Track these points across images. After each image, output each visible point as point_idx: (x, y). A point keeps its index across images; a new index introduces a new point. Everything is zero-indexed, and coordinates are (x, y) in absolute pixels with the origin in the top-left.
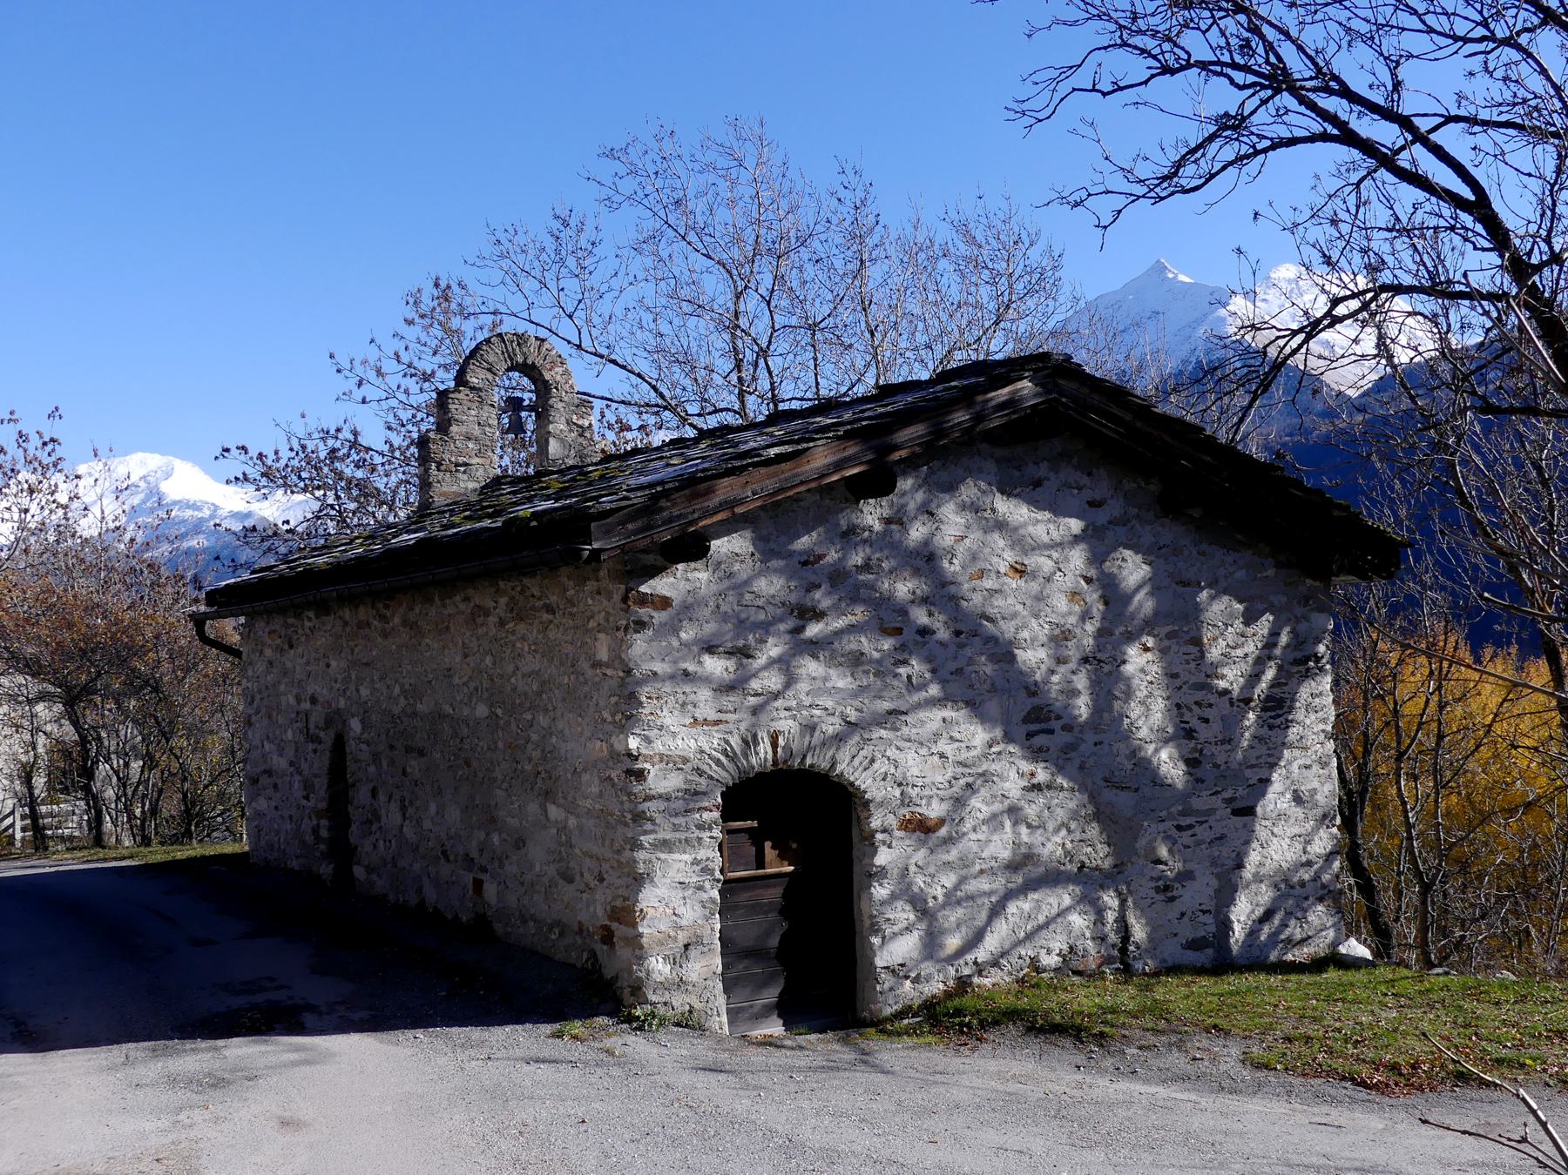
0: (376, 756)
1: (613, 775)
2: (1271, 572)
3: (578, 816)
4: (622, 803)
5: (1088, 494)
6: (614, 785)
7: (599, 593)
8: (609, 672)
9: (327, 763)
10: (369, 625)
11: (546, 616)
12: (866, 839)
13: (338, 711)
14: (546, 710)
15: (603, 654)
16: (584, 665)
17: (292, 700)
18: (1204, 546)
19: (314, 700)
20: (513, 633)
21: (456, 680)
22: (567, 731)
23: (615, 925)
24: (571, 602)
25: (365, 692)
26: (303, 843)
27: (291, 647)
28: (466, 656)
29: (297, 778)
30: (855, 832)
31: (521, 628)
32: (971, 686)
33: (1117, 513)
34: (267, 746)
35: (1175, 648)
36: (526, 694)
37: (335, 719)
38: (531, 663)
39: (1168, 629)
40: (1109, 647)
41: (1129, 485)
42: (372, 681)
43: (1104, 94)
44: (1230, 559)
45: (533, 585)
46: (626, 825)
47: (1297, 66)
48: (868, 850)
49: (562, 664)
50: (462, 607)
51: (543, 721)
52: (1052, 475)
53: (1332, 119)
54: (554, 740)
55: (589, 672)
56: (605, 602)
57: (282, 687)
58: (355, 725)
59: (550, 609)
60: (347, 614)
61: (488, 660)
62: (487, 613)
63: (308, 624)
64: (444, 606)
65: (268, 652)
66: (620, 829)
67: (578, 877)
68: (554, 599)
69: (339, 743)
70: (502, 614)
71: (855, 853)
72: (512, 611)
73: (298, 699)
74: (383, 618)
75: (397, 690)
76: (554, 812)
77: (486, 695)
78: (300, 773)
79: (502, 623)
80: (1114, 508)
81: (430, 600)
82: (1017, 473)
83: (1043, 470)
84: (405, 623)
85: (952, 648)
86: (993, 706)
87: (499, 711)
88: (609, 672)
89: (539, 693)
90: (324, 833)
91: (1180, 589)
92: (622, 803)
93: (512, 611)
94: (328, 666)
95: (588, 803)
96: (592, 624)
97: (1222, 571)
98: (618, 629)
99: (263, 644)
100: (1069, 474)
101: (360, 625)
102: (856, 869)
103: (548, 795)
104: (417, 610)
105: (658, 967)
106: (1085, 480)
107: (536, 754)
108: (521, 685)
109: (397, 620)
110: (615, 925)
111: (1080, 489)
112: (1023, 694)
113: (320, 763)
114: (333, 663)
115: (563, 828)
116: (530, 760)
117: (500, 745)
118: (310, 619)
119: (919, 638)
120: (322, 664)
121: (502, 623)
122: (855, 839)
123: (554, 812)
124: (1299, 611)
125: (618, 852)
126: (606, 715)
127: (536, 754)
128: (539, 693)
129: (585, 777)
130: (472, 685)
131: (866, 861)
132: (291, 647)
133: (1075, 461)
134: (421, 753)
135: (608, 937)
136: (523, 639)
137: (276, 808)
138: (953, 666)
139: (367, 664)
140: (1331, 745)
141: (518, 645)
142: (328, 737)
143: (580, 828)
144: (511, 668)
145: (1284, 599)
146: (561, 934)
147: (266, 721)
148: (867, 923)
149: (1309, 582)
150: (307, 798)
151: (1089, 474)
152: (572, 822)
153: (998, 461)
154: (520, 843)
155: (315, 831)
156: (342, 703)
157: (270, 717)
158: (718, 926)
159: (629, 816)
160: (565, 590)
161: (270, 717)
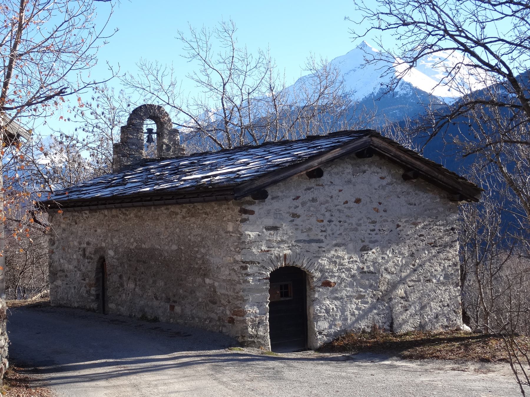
0: (122, 264)
1: (235, 268)
2: (438, 200)
3: (219, 282)
4: (239, 277)
5: (380, 175)
6: (235, 271)
7: (228, 209)
8: (233, 235)
9: (95, 266)
10: (117, 216)
11: (204, 216)
12: (311, 289)
13: (102, 248)
14: (204, 247)
15: (230, 229)
16: (222, 232)
17: (76, 243)
18: (417, 192)
19: (88, 243)
20: (189, 221)
21: (162, 237)
22: (214, 254)
23: (235, 317)
24: (216, 211)
25: (115, 241)
26: (82, 296)
27: (76, 224)
28: (166, 228)
29: (79, 272)
30: (308, 287)
31: (193, 219)
32: (344, 239)
33: (389, 181)
34: (62, 261)
35: (408, 226)
36: (195, 242)
37: (99, 250)
38: (197, 231)
39: (406, 219)
40: (387, 226)
41: (393, 172)
42: (119, 237)
43: (383, 30)
44: (425, 196)
45: (199, 206)
46: (240, 284)
47: (450, 28)
48: (312, 293)
49: (212, 232)
50: (165, 211)
51: (203, 250)
52: (369, 169)
53: (462, 44)
54: (208, 257)
55: (224, 235)
56: (231, 212)
57: (71, 239)
58: (111, 253)
59: (206, 213)
60: (106, 212)
61: (177, 230)
62: (177, 214)
63: (85, 215)
64: (156, 211)
65: (63, 226)
66: (238, 285)
67: (218, 302)
68: (208, 210)
69: (102, 261)
70: (184, 215)
71: (308, 294)
72: (188, 213)
73: (80, 243)
74: (125, 214)
75: (132, 240)
76: (207, 281)
77: (176, 242)
78: (80, 271)
79: (184, 217)
80: (389, 179)
81: (150, 210)
82: (358, 169)
83: (366, 167)
84: (136, 216)
85: (339, 226)
86: (351, 246)
87: (182, 248)
88: (233, 235)
89: (201, 242)
90: (93, 292)
91: (409, 206)
92: (239, 277)
93: (188, 213)
94: (96, 231)
95: (224, 278)
96: (225, 219)
97: (423, 200)
98: (237, 221)
99: (60, 222)
100: (374, 169)
101: (113, 216)
102: (308, 299)
103: (205, 275)
104: (142, 212)
105: (251, 331)
106: (379, 170)
107: (200, 262)
108: (193, 239)
109: (132, 215)
110: (235, 317)
111: (377, 173)
112: (360, 241)
113: (90, 267)
114: (99, 230)
115: (212, 286)
116: (197, 263)
117: (183, 259)
118: (86, 214)
119: (328, 223)
120: (92, 231)
121: (184, 217)
122: (308, 289)
123: (207, 281)
124: (447, 213)
125: (237, 293)
126: (232, 249)
127: (200, 262)
128: (201, 242)
129: (222, 269)
130: (169, 239)
131: (312, 296)
132: (76, 224)
133: (376, 164)
134: (144, 262)
135: (232, 321)
136: (194, 223)
137: (67, 284)
138: (339, 232)
139: (117, 231)
140: (458, 258)
141: (192, 225)
142: (96, 258)
143: (220, 286)
144: (188, 233)
145: (443, 209)
146: (210, 322)
147: (61, 252)
148: (312, 316)
149: (451, 203)
150: (84, 280)
151: (381, 168)
152: (216, 284)
153: (352, 165)
154: (193, 292)
155: (88, 292)
156: (104, 245)
157: (64, 250)
158: (268, 317)
159: (242, 281)
160: (214, 207)
161: (64, 250)
